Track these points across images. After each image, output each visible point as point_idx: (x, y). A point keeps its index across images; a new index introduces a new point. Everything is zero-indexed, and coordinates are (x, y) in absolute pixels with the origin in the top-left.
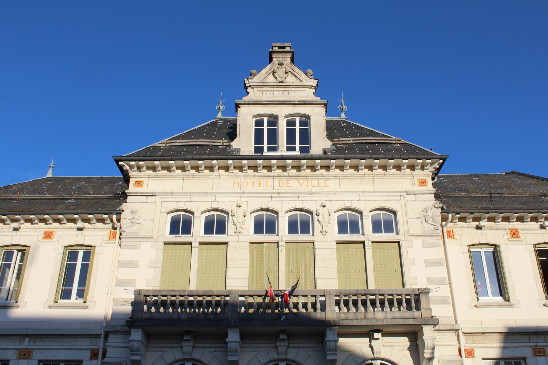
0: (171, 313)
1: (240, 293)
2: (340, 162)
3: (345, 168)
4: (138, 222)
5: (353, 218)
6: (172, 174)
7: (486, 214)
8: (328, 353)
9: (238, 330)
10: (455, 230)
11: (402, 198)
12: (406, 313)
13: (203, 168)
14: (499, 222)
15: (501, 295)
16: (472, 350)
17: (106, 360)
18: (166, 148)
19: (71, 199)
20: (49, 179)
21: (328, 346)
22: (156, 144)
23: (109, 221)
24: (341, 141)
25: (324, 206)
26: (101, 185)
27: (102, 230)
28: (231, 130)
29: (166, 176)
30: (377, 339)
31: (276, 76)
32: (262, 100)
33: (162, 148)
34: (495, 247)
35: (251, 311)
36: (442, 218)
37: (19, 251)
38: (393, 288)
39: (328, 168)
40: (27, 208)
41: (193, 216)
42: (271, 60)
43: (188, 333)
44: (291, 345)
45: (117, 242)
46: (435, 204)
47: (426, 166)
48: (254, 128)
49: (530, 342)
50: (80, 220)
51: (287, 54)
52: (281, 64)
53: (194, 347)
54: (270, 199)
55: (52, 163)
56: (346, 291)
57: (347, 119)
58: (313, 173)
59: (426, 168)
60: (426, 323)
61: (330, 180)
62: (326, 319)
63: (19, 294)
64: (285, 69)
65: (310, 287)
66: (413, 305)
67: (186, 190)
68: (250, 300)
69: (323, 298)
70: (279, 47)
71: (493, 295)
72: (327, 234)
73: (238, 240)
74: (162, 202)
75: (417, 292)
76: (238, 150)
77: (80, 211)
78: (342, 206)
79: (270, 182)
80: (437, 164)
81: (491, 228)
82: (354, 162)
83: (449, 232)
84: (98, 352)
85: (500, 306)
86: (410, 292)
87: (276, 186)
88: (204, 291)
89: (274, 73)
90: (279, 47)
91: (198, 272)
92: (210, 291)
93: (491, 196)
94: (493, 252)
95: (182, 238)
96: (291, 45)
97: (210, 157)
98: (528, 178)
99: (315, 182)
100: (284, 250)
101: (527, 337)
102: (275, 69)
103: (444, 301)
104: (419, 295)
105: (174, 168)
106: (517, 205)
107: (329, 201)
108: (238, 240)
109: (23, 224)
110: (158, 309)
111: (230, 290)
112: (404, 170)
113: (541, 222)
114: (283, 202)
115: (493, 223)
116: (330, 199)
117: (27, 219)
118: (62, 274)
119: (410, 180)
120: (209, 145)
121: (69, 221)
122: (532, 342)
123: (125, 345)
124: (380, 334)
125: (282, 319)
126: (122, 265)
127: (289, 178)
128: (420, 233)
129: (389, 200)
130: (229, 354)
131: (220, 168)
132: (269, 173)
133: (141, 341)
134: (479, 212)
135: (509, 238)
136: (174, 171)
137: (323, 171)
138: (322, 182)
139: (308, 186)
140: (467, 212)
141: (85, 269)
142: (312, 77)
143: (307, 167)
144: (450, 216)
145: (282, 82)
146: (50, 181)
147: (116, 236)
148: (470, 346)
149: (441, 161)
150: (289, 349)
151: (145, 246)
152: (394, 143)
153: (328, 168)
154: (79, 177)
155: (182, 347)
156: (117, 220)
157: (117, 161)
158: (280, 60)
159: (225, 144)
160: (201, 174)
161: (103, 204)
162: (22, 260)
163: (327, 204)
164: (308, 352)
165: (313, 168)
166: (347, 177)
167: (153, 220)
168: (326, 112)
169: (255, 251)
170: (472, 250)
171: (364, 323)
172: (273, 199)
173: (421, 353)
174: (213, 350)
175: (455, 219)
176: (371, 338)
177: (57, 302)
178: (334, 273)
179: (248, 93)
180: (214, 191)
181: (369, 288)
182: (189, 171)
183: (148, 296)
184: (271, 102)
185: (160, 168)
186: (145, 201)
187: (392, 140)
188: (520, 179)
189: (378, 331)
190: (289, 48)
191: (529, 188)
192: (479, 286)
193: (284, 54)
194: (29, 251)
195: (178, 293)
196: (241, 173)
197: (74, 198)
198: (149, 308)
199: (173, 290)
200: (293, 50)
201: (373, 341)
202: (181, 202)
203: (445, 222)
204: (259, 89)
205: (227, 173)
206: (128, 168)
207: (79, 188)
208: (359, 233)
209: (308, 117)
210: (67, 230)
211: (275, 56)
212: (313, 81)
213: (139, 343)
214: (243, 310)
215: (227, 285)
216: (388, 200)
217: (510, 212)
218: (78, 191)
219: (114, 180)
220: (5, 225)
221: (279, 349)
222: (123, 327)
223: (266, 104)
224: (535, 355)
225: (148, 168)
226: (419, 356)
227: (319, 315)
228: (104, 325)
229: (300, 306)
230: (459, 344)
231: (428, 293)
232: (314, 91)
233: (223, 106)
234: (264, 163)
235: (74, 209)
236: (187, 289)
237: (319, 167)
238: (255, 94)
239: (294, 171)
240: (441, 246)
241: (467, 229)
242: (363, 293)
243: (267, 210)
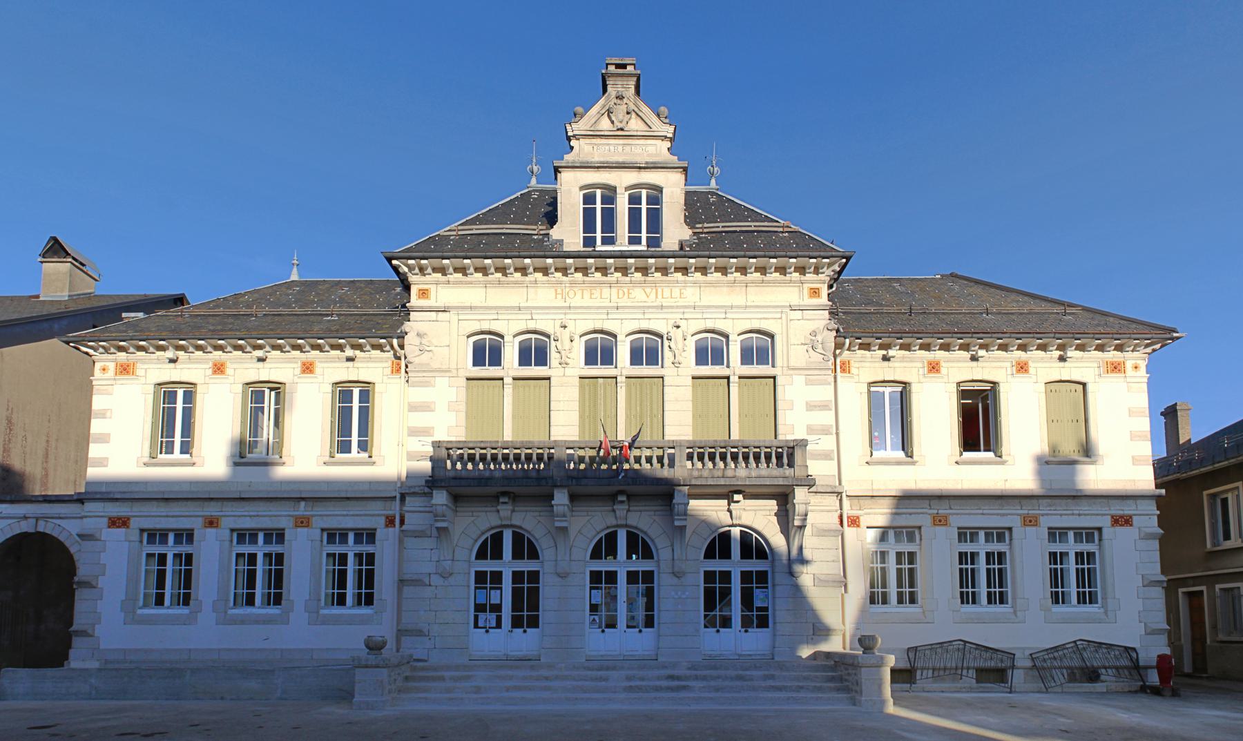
0: (470, 470)
1: (567, 445)
2: (701, 262)
3: (708, 271)
4: (428, 349)
5: (717, 344)
6: (469, 278)
7: (898, 339)
8: (676, 517)
9: (566, 491)
10: (852, 362)
11: (784, 316)
12: (775, 471)
13: (512, 270)
14: (915, 351)
15: (903, 449)
16: (858, 517)
17: (404, 527)
18: (457, 237)
19: (332, 315)
20: (295, 283)
21: (676, 510)
22: (441, 232)
23: (388, 348)
24: (705, 228)
25: (678, 327)
26: (371, 293)
27: (381, 360)
28: (551, 208)
29: (462, 282)
30: (738, 502)
31: (613, 118)
32: (593, 160)
33: (452, 238)
34: (992, 385)
35: (582, 466)
36: (835, 344)
37: (271, 389)
38: (762, 438)
39: (685, 271)
40: (271, 330)
41: (502, 341)
42: (605, 90)
43: (504, 494)
44: (631, 508)
45: (403, 378)
46: (828, 324)
47: (822, 268)
48: (582, 206)
49: (930, 509)
50: (348, 346)
51: (630, 78)
52: (620, 97)
53: (513, 511)
54: (605, 317)
55: (295, 258)
56: (701, 441)
57: (718, 190)
58: (665, 278)
59: (821, 271)
60: (799, 484)
61: (687, 289)
62: (676, 477)
63: (282, 447)
64: (626, 106)
65: (657, 437)
66: (785, 460)
67: (490, 303)
68: (581, 453)
69: (672, 451)
70: (618, 66)
71: (893, 449)
72: (681, 366)
74: (459, 320)
75: (792, 445)
76: (561, 242)
77: (346, 333)
78: (702, 327)
79: (606, 291)
80: (837, 264)
81: (903, 359)
82: (722, 262)
83: (843, 364)
84: (395, 518)
85: (899, 463)
86: (781, 445)
87: (614, 297)
88: (522, 442)
89: (609, 112)
90: (618, 66)
91: (514, 417)
92: (530, 442)
93: (910, 312)
94: (901, 392)
95: (489, 371)
96: (634, 62)
97: (521, 253)
98: (972, 284)
99: (667, 292)
100: (624, 388)
101: (927, 502)
102: (611, 106)
103: (826, 456)
104: (793, 448)
105: (472, 270)
106: (944, 326)
107: (685, 319)
109: (269, 352)
110: (464, 465)
111: (555, 441)
112: (791, 273)
113: (974, 351)
115: (907, 352)
116: (686, 316)
117: (274, 344)
118: (335, 419)
119: (797, 289)
120: (519, 234)
121: (333, 347)
122: (934, 509)
123: (427, 509)
124: (741, 496)
125: (620, 477)
126: (413, 408)
127: (631, 285)
128: (803, 365)
129: (766, 319)
130: (556, 519)
131: (536, 270)
132: (604, 278)
133: (446, 505)
134: (889, 337)
135: (1014, 373)
136: (472, 274)
137: (679, 275)
138: (676, 292)
139: (657, 297)
140: (872, 337)
141: (365, 414)
142: (667, 121)
143: (656, 268)
144: (847, 341)
145: (622, 129)
146: (297, 286)
147: (400, 368)
148: (854, 513)
149: (844, 260)
150: (629, 513)
151: (442, 382)
152: (781, 232)
153: (684, 270)
154: (338, 279)
155: (498, 511)
156: (399, 346)
157: (389, 260)
158: (619, 89)
159: (542, 232)
160: (510, 278)
161: (378, 323)
162: (277, 403)
163: (682, 323)
164: (653, 517)
165: (664, 271)
166: (711, 284)
167: (449, 346)
168: (686, 180)
169: (587, 388)
170: (873, 389)
171: (722, 482)
172: (610, 316)
173: (790, 519)
174: (537, 514)
175: (854, 346)
176: (731, 501)
177: (333, 457)
178: (688, 418)
179: (572, 148)
180: (529, 304)
181: (732, 438)
182: (493, 274)
183: (451, 449)
184: (605, 165)
185: (451, 270)
186: (435, 319)
187: (779, 227)
188: (960, 286)
189: (738, 492)
190: (633, 67)
191: (969, 300)
192: (876, 437)
193: (625, 79)
194: (285, 390)
195: (488, 445)
196: (565, 278)
197: (336, 314)
198: (454, 464)
199: (482, 441)
200: (639, 72)
201: (732, 504)
203: (840, 350)
204: (588, 141)
205: (545, 278)
206: (406, 270)
207: (340, 297)
208: (723, 364)
209: (613, 189)
210: (333, 360)
211: (611, 83)
212: (668, 127)
213: (444, 507)
214: (572, 466)
215: (552, 433)
216: (764, 318)
217: (932, 337)
218: (339, 302)
219: (388, 285)
220: (225, 354)
221: (617, 512)
222: (422, 488)
223: (598, 167)
224: (934, 525)
225: (435, 270)
226: (788, 523)
227: (666, 473)
228: (399, 485)
229: (643, 460)
230: (841, 509)
231: (806, 446)
232: (669, 144)
233: (538, 166)
234: (637, 263)
235: (337, 331)
236: (500, 440)
237: (673, 270)
238: (583, 149)
239: (638, 275)
240: (829, 384)
241: (870, 360)
242: (722, 445)
243: (602, 332)
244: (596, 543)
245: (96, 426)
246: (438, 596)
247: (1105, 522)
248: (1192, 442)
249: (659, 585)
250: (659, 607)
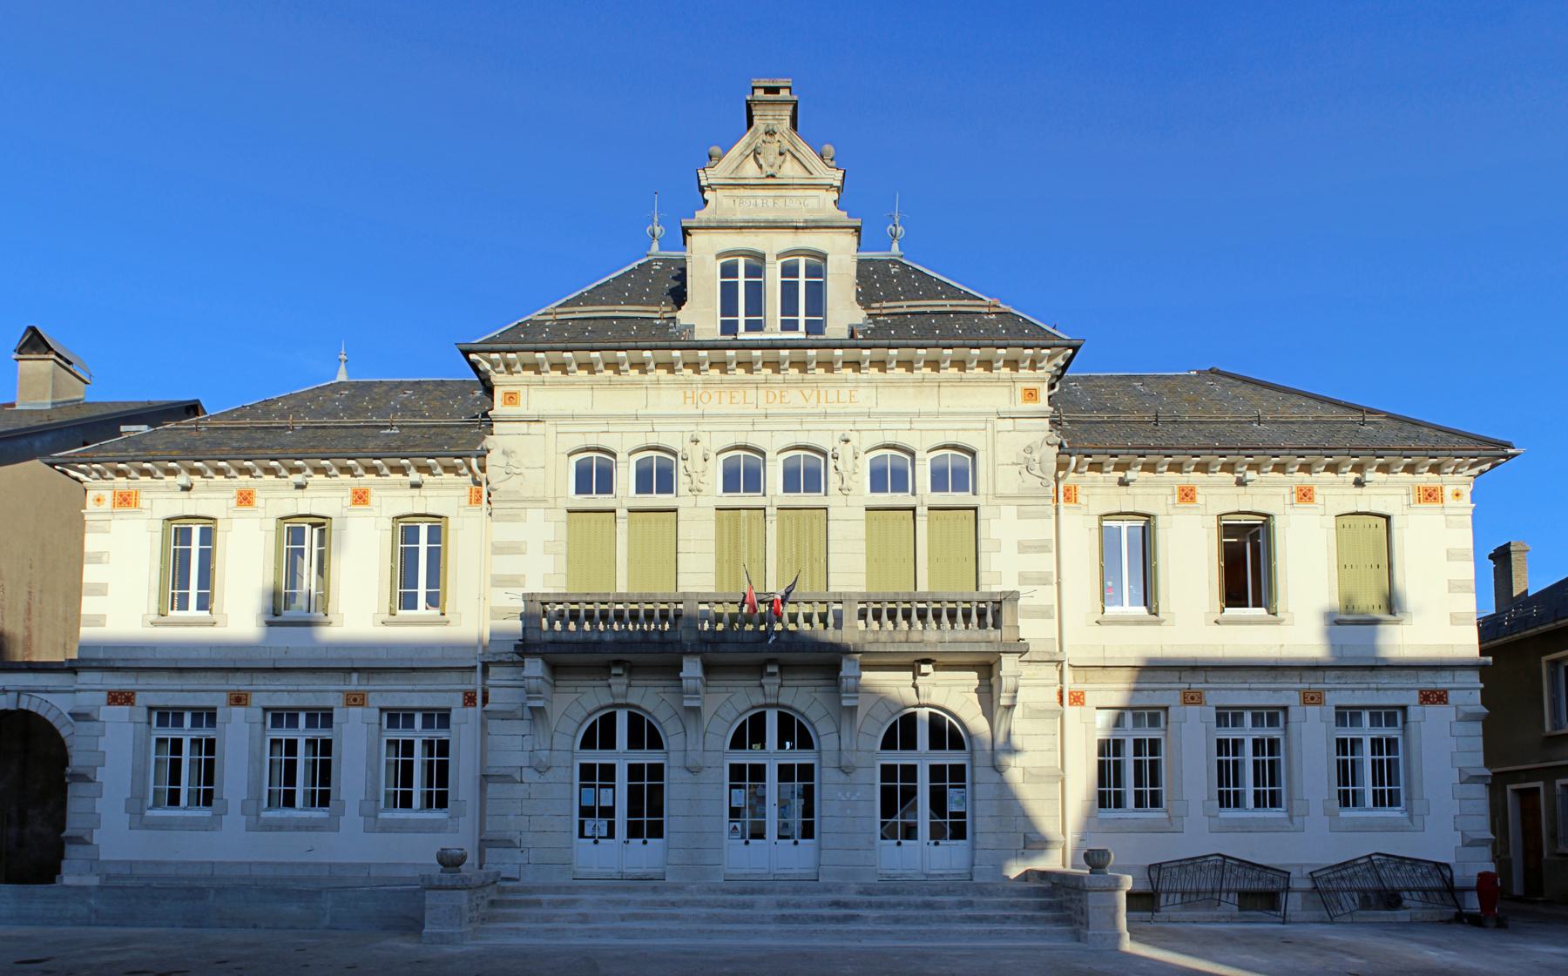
66: (989, 619)
245: (90, 574)
247: (454, 701)
248: (1529, 595)
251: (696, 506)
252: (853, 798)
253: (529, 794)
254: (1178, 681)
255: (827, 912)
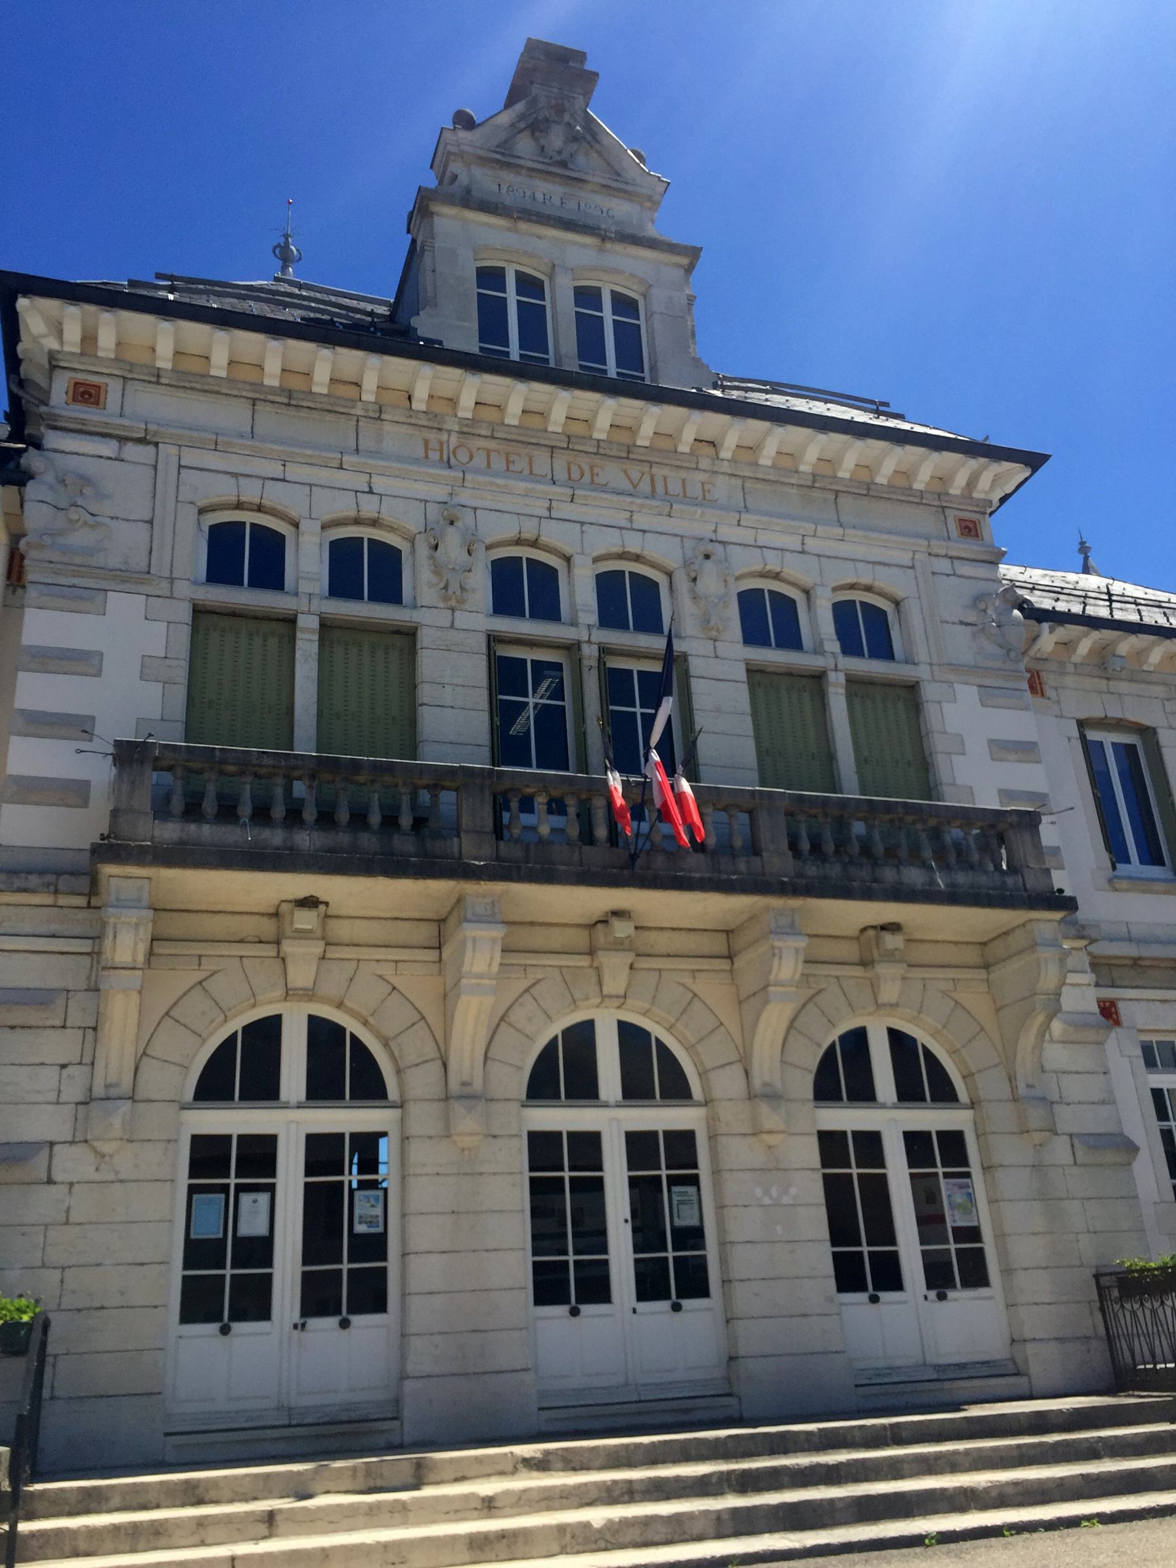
73: (453, 623)
108: (453, 623)
114: (585, 528)
202: (249, 479)
244: (943, 1069)
246: (75, 1217)
248: (8, 411)
249: (716, 1172)
250: (404, 1240)
251: (452, 626)
252: (786, 1200)
253: (68, 1211)
254: (197, 967)
255: (598, 1516)
